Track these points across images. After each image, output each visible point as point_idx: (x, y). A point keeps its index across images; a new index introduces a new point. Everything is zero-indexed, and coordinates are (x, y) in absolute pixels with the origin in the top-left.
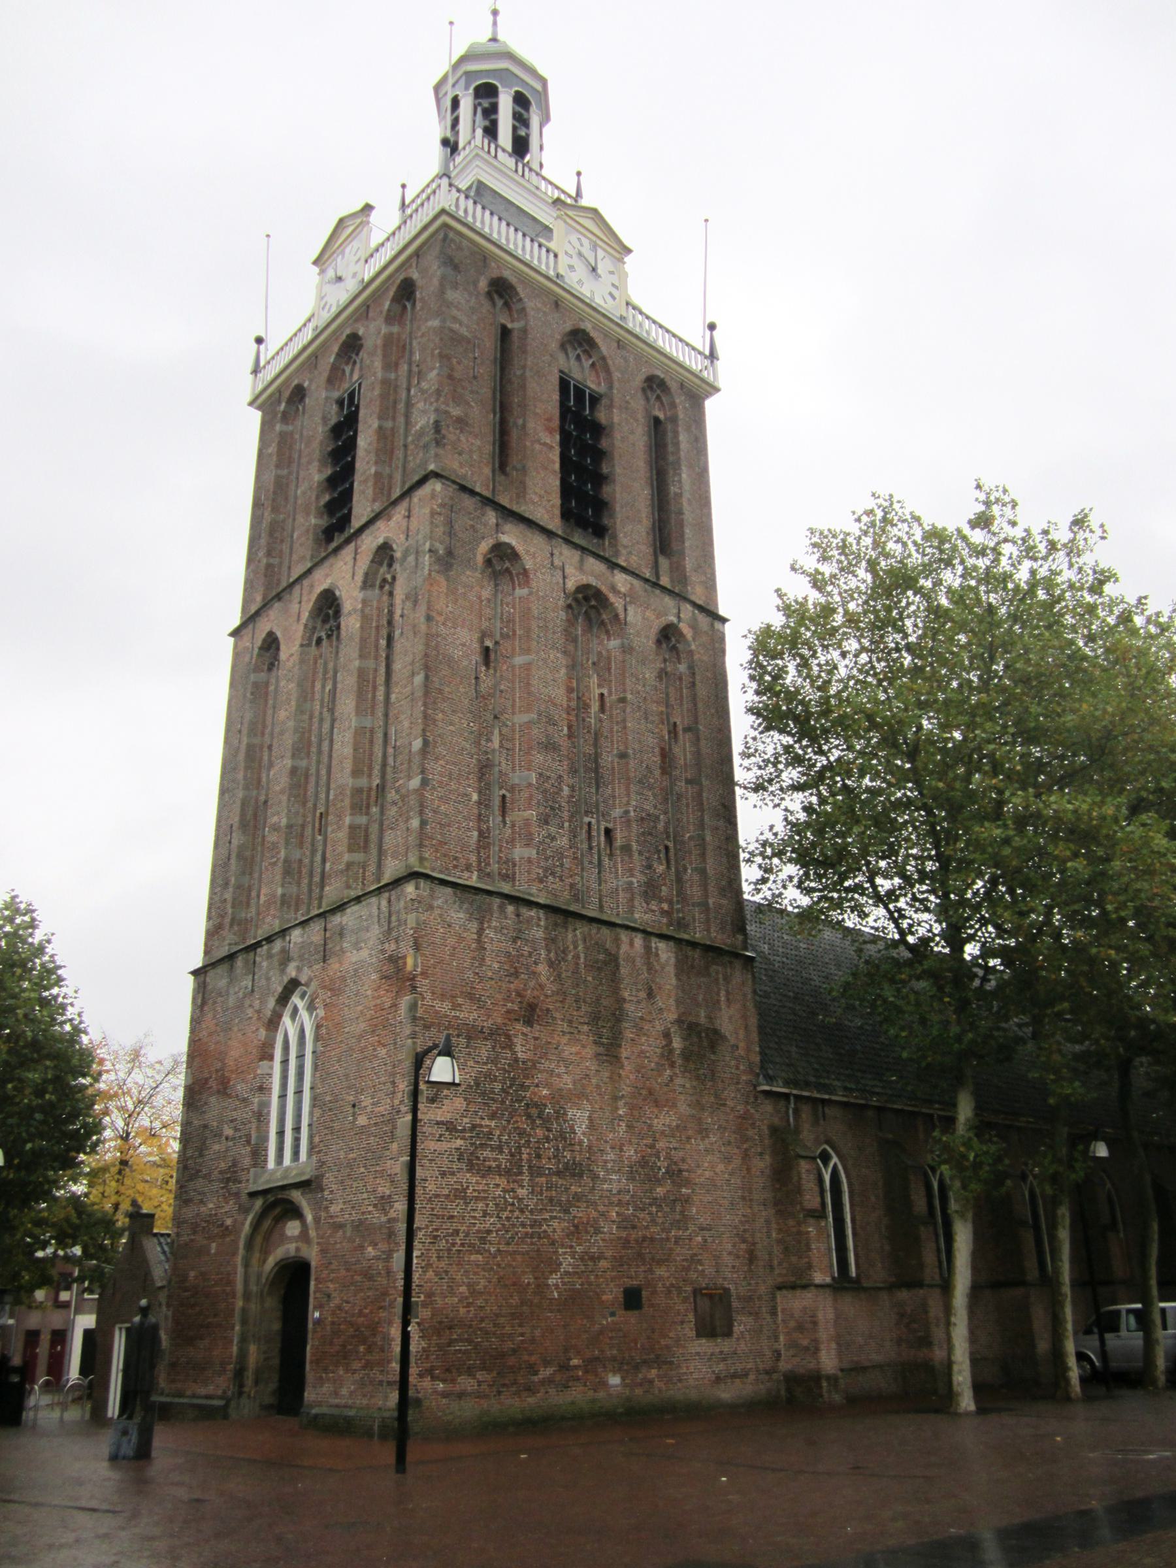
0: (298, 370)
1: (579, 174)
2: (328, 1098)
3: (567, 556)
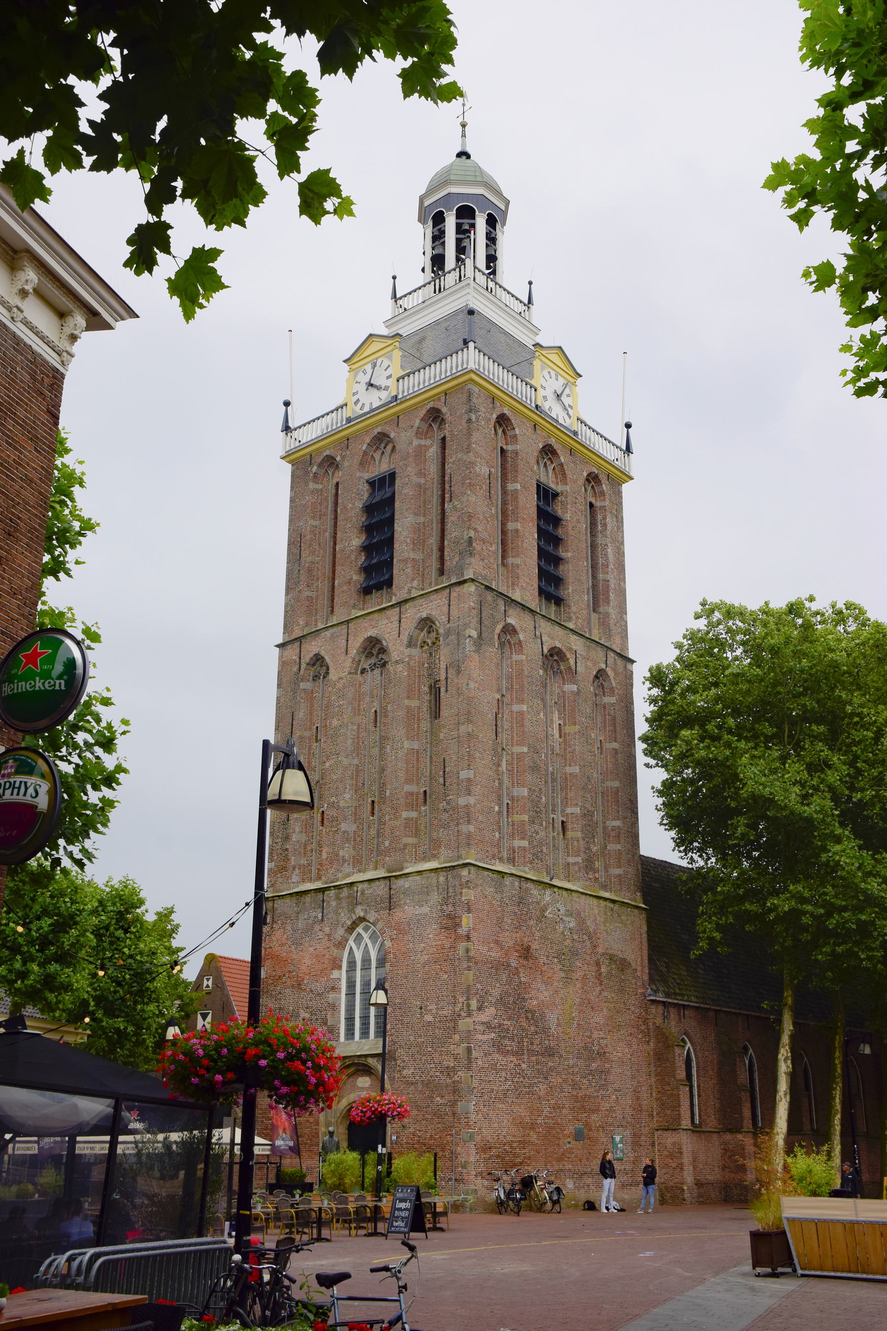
1: (530, 283)
2: (398, 1001)
3: (545, 627)
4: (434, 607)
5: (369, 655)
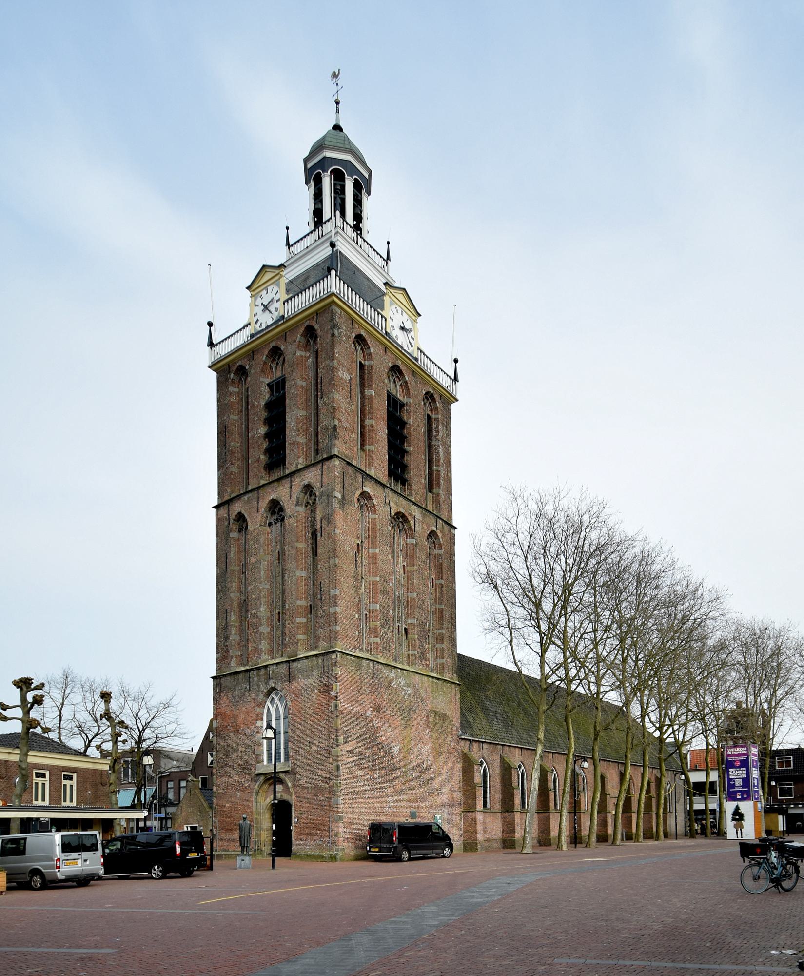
0: (240, 356)
4: (311, 477)
5: (273, 513)
